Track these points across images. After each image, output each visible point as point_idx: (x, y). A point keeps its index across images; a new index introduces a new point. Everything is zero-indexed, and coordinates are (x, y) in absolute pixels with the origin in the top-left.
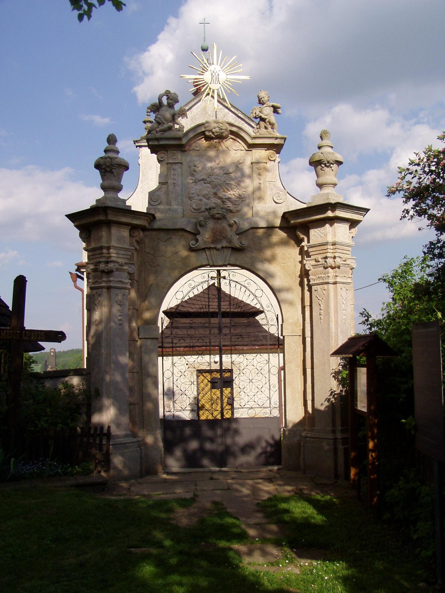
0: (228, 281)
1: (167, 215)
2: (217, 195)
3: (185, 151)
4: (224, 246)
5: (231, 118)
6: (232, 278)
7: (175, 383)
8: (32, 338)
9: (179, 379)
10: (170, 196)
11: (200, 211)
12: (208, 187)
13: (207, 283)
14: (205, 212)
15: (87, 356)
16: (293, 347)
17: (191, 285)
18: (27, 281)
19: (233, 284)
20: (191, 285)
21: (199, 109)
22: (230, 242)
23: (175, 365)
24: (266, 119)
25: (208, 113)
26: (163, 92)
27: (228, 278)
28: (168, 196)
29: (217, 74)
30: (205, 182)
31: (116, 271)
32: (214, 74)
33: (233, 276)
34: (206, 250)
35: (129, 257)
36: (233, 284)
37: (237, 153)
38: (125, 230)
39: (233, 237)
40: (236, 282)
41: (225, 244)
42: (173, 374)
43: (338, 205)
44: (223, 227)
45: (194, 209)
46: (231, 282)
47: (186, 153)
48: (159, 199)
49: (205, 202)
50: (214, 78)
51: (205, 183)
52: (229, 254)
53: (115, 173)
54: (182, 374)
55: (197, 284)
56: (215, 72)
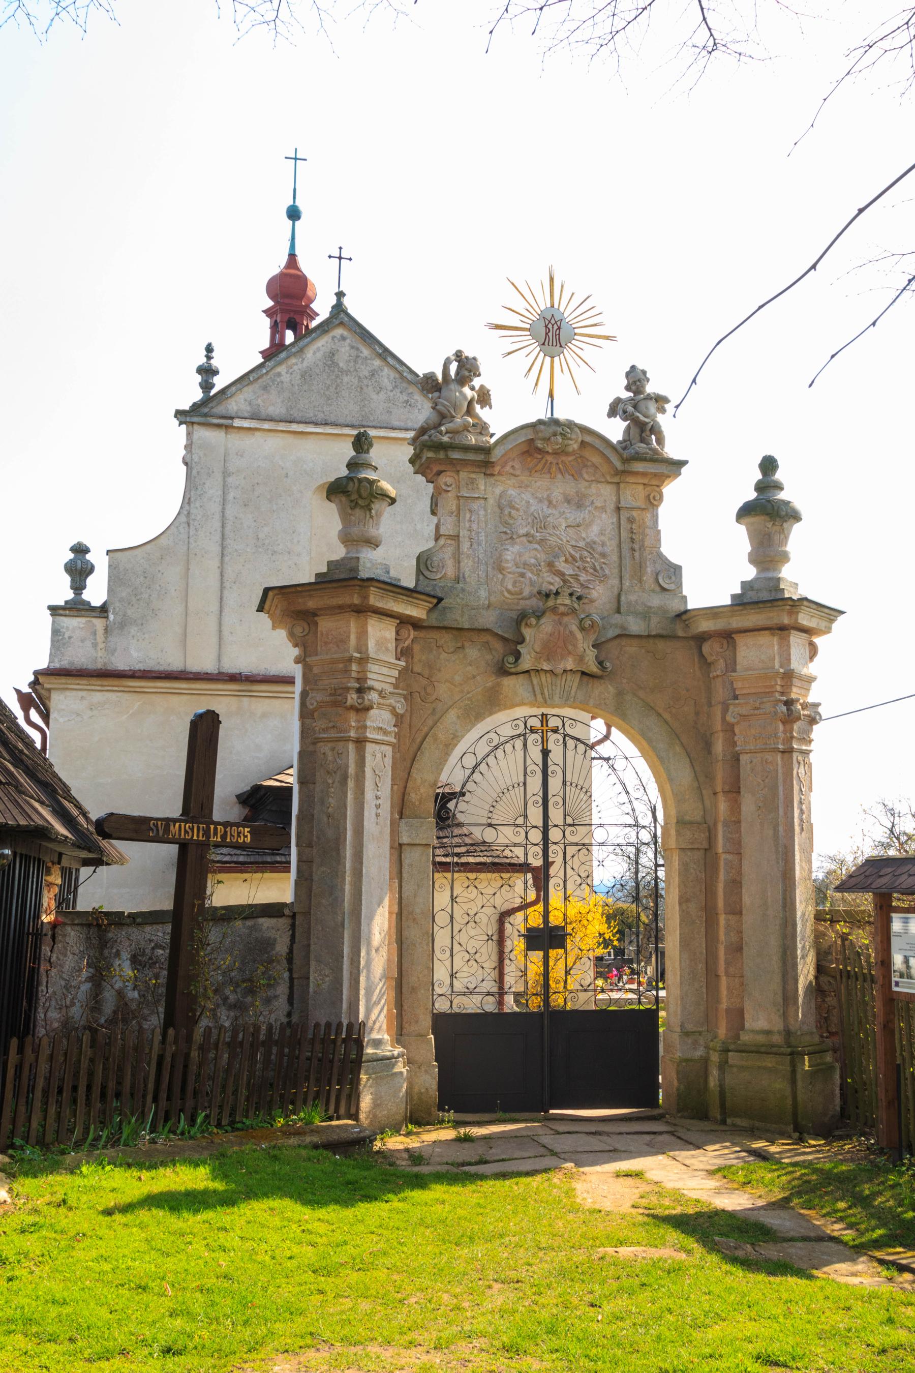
0: (561, 738)
1: (459, 600)
2: (553, 566)
3: (492, 475)
4: (569, 669)
5: (386, 380)
6: (569, 731)
7: (457, 938)
8: (228, 840)
9: (464, 929)
10: (462, 564)
11: (520, 597)
12: (536, 549)
13: (522, 738)
14: (529, 598)
15: (298, 877)
16: (692, 871)
17: (491, 741)
18: (220, 722)
19: (571, 743)
20: (491, 741)
21: (319, 355)
22: (581, 659)
23: (457, 900)
24: (647, 423)
25: (338, 364)
26: (451, 353)
27: (562, 731)
28: (459, 563)
29: (556, 327)
30: (531, 539)
31: (378, 708)
32: (550, 326)
33: (571, 726)
34: (533, 674)
35: (394, 681)
36: (571, 743)
37: (590, 487)
38: (390, 627)
39: (588, 652)
40: (578, 740)
41: (570, 664)
42: (452, 917)
43: (805, 603)
44: (571, 632)
45: (509, 592)
46: (567, 738)
47: (492, 480)
48: (443, 567)
49: (530, 579)
50: (550, 334)
51: (530, 542)
52: (576, 684)
53: (373, 511)
54: (472, 919)
55: (502, 739)
56: (553, 321)
